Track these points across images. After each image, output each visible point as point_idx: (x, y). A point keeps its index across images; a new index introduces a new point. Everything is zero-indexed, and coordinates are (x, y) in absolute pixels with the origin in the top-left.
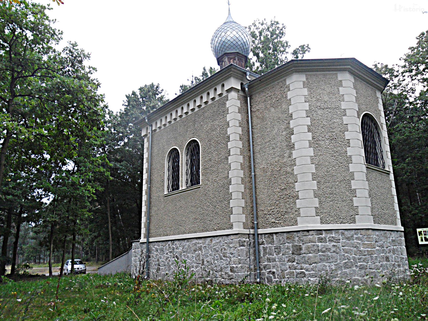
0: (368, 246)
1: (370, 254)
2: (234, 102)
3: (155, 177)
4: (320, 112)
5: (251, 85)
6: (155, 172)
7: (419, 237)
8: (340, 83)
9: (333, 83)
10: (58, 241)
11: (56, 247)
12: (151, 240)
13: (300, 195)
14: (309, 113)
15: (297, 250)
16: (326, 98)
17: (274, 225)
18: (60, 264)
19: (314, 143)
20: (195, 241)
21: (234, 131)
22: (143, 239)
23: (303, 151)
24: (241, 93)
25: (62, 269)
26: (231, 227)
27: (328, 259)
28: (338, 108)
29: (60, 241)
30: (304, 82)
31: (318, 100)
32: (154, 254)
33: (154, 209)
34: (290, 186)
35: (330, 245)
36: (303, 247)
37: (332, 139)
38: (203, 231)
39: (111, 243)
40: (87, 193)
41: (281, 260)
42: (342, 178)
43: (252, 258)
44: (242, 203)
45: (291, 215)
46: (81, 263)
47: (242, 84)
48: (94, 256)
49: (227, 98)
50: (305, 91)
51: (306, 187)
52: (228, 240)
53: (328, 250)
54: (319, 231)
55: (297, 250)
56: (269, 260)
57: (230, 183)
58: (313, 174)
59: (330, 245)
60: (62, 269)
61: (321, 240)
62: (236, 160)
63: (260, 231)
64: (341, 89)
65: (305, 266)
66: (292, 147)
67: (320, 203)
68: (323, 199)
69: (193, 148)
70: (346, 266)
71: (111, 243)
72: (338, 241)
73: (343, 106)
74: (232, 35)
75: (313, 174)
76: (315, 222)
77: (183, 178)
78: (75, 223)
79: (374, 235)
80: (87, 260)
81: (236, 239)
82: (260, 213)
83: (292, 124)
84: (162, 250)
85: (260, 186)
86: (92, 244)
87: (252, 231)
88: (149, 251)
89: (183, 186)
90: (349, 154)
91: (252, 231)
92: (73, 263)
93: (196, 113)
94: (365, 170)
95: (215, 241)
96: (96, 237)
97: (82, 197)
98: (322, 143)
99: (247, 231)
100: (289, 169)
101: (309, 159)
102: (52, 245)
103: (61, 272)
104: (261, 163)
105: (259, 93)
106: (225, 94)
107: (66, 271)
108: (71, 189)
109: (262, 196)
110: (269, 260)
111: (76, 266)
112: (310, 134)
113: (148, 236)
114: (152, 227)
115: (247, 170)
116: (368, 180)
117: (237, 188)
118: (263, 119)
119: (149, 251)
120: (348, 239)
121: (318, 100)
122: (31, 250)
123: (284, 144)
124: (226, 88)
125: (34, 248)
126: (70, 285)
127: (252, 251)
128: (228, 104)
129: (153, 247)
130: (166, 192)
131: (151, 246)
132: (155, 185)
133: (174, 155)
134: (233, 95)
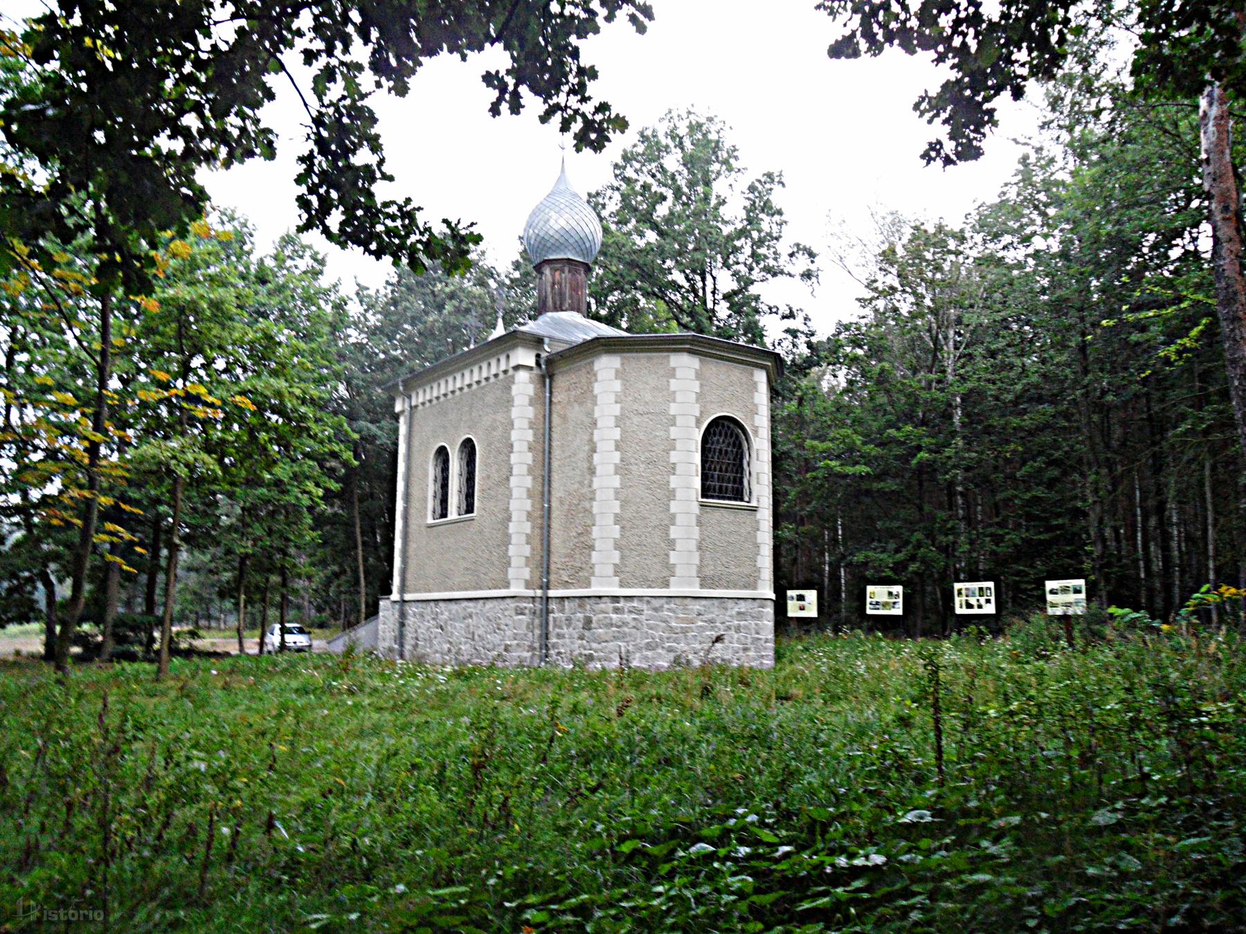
0: (683, 620)
1: (684, 631)
2: (524, 385)
3: (415, 491)
4: (636, 419)
5: (550, 361)
6: (414, 480)
7: (957, 600)
8: (672, 373)
9: (662, 372)
10: (254, 587)
11: (249, 601)
12: (408, 597)
13: (597, 545)
14: (620, 421)
15: (588, 623)
16: (648, 397)
17: (566, 585)
18: (258, 632)
19: (622, 469)
20: (465, 604)
21: (522, 436)
22: (395, 596)
23: (607, 481)
24: (536, 371)
25: (262, 644)
26: (507, 586)
27: (623, 637)
28: (664, 413)
29: (257, 587)
30: (617, 371)
31: (635, 400)
32: (411, 620)
33: (413, 546)
34: (587, 531)
35: (627, 617)
36: (594, 619)
37: (650, 462)
38: (475, 588)
39: (363, 590)
40: (305, 500)
41: (571, 637)
42: (657, 523)
43: (537, 632)
44: (527, 551)
45: (582, 574)
46: (301, 631)
47: (538, 356)
48: (335, 616)
49: (512, 380)
50: (617, 385)
51: (605, 532)
52: (503, 604)
53: (625, 624)
54: (615, 599)
55: (588, 623)
56: (559, 636)
57: (509, 519)
58: (616, 515)
59: (627, 617)
60: (262, 644)
61: (616, 610)
62: (521, 482)
63: (552, 593)
64: (672, 381)
65: (594, 645)
66: (592, 471)
67: (622, 558)
68: (627, 553)
69: (468, 448)
70: (649, 647)
71: (363, 590)
72: (640, 612)
73: (673, 409)
74: (557, 227)
75: (616, 515)
76: (610, 585)
77: (454, 500)
78: (285, 554)
79: (697, 606)
80: (322, 626)
81: (512, 604)
82: (553, 567)
83: (597, 435)
84: (422, 615)
85: (555, 524)
86: (327, 592)
87: (539, 593)
88: (403, 615)
89: (453, 514)
90: (672, 485)
91: (539, 593)
92: (284, 631)
93: (474, 394)
94: (696, 509)
95: (489, 605)
96: (336, 575)
97: (296, 508)
98: (634, 468)
99: (530, 593)
100: (587, 505)
101: (612, 492)
102: (243, 597)
103: (261, 650)
104: (558, 492)
105: (563, 373)
106: (511, 372)
107: (270, 648)
108: (274, 493)
109: (556, 541)
110: (559, 636)
111: (289, 638)
112: (618, 454)
113: (403, 589)
114: (409, 576)
115: (538, 498)
116: (700, 523)
117: (520, 527)
118: (564, 418)
119: (403, 615)
120: (656, 610)
121: (635, 400)
122: (189, 597)
123: (586, 465)
124: (513, 363)
125: (195, 593)
126: (275, 664)
127: (537, 621)
128: (515, 390)
129: (411, 610)
130: (430, 521)
131: (407, 607)
132: (415, 504)
133: (442, 453)
134: (522, 376)
